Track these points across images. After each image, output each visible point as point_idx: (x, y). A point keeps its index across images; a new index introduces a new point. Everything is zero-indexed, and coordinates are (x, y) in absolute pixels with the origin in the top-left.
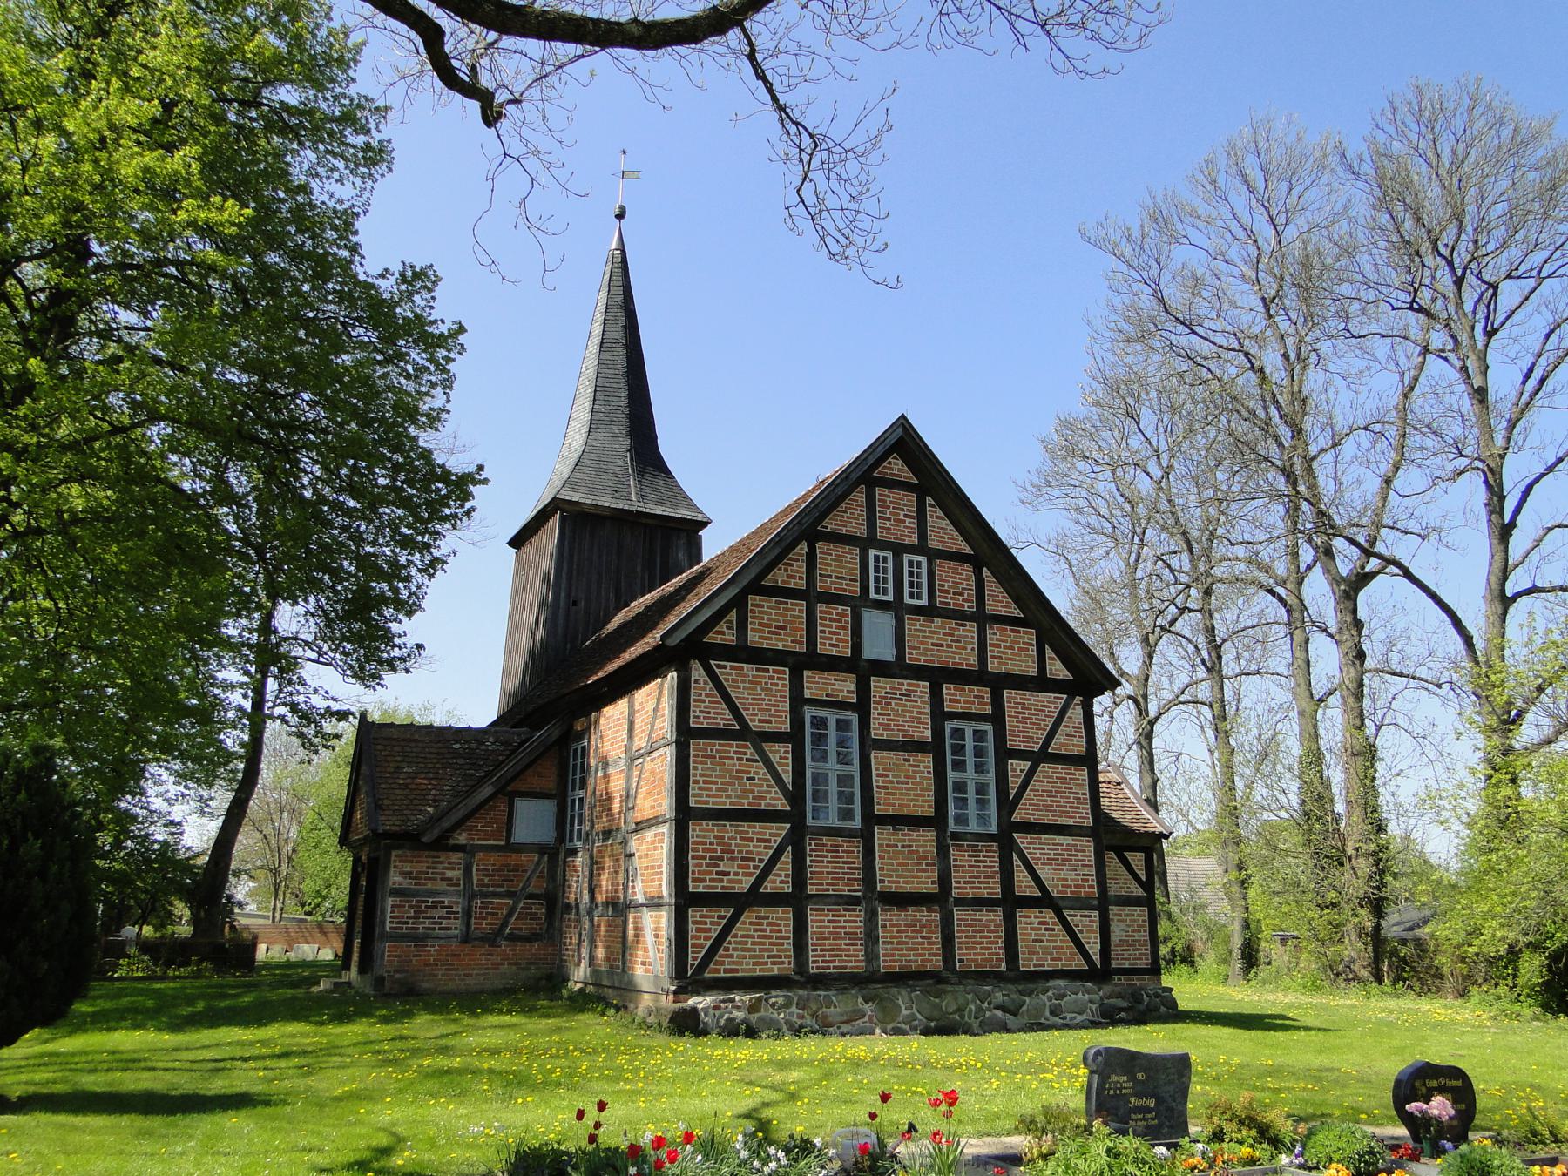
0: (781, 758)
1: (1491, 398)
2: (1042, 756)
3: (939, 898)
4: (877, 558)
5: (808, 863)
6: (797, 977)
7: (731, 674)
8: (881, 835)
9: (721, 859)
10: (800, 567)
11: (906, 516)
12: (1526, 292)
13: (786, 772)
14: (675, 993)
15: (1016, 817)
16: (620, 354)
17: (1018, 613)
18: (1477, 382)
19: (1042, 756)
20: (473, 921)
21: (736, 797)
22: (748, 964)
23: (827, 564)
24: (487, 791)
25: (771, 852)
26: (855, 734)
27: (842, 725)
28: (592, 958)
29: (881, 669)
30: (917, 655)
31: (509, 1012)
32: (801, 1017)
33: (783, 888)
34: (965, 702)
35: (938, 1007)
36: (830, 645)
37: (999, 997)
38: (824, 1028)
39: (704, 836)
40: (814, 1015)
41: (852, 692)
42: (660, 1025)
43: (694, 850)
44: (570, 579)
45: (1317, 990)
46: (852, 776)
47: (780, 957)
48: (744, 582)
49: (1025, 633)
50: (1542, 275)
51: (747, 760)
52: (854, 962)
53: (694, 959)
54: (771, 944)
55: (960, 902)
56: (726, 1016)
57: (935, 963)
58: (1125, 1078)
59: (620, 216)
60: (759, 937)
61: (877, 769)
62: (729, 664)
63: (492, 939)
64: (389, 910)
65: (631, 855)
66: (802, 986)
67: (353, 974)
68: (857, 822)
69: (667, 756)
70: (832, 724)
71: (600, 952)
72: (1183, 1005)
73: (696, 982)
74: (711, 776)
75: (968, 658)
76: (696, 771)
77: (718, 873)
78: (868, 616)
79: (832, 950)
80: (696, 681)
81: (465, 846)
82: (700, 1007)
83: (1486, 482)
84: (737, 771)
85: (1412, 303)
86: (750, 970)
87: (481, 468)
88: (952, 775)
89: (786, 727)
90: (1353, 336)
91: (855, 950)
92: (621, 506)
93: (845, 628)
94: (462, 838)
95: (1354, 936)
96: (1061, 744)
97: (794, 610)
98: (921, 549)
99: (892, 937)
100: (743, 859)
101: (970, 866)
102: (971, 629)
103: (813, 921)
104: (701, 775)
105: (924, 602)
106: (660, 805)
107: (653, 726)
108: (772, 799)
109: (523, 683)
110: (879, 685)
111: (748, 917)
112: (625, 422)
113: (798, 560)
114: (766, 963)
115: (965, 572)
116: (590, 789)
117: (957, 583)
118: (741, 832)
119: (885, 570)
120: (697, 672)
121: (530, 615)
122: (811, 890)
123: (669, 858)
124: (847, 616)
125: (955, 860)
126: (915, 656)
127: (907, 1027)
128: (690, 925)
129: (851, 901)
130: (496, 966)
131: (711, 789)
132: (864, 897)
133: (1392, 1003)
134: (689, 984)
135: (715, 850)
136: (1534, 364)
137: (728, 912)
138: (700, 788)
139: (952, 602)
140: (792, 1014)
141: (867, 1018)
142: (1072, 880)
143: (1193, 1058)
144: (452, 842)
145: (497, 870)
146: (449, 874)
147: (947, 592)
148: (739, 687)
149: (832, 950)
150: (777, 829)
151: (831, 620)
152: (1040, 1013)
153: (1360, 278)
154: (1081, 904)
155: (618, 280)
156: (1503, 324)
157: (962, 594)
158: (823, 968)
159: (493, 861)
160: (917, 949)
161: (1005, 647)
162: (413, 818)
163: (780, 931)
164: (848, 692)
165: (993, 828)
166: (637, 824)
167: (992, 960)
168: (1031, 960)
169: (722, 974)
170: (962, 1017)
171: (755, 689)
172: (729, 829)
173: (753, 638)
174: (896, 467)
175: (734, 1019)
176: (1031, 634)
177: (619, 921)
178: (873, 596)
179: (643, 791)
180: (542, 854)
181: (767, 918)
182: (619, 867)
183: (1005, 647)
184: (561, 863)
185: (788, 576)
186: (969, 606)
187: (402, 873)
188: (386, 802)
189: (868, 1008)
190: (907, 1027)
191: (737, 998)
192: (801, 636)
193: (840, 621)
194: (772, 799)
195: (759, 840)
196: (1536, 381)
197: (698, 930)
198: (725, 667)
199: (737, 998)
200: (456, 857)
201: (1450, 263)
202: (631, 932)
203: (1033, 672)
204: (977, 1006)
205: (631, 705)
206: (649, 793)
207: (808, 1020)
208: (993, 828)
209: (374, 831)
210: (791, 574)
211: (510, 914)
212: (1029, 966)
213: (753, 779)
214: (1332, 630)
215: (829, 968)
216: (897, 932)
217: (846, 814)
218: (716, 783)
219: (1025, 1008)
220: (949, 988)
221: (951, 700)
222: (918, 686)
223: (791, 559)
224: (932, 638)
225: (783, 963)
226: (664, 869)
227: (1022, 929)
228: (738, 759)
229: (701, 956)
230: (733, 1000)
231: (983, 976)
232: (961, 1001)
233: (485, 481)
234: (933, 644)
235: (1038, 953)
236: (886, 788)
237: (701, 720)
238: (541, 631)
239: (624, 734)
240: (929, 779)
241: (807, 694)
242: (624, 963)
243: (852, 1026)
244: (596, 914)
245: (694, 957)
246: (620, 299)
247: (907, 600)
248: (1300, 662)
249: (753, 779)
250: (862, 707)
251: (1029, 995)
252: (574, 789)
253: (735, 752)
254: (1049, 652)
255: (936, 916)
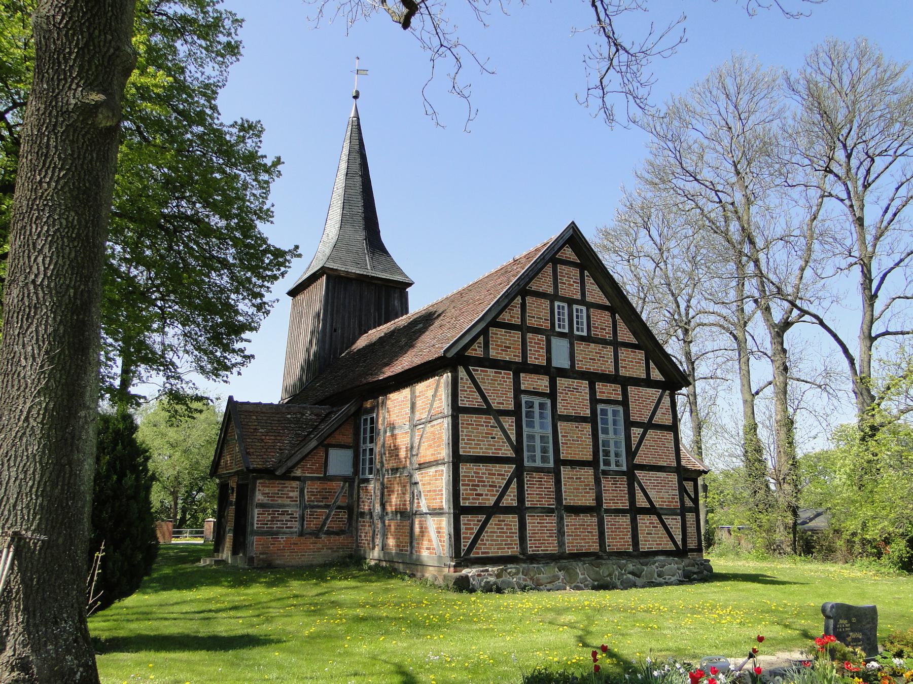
0: (509, 425)
1: (865, 224)
2: (649, 426)
3: (596, 509)
4: (559, 306)
5: (526, 488)
6: (521, 556)
7: (481, 375)
8: (565, 471)
9: (478, 486)
10: (517, 311)
11: (574, 282)
12: (887, 164)
13: (512, 434)
14: (455, 566)
15: (636, 461)
16: (358, 180)
17: (635, 341)
18: (858, 215)
19: (649, 426)
20: (305, 522)
21: (486, 449)
22: (494, 549)
23: (532, 310)
24: (314, 443)
25: (505, 482)
26: (548, 412)
27: (542, 406)
28: (384, 547)
29: (562, 373)
30: (582, 365)
31: (346, 579)
32: (525, 580)
33: (512, 503)
34: (608, 393)
35: (598, 573)
36: (535, 358)
37: (630, 567)
38: (537, 587)
39: (469, 472)
40: (532, 579)
41: (547, 387)
42: (447, 586)
43: (463, 481)
44: (332, 315)
45: (764, 559)
46: (548, 437)
47: (512, 544)
48: (489, 319)
49: (639, 353)
50: (897, 154)
51: (491, 426)
52: (552, 547)
53: (464, 546)
54: (507, 537)
55: (608, 511)
56: (485, 580)
57: (595, 547)
58: (846, 621)
59: (356, 97)
60: (500, 532)
61: (561, 433)
62: (479, 369)
63: (316, 534)
64: (256, 516)
65: (416, 483)
66: (524, 561)
67: (226, 554)
68: (551, 464)
69: (446, 423)
70: (536, 406)
71: (391, 542)
72: (716, 570)
73: (466, 559)
74: (471, 436)
75: (608, 367)
76: (463, 433)
77: (477, 495)
78: (555, 341)
79: (540, 540)
80: (462, 379)
81: (300, 477)
82: (470, 575)
83: (862, 271)
84: (486, 433)
85: (826, 167)
86: (495, 552)
87: (297, 247)
88: (601, 437)
89: (511, 407)
90: (789, 186)
91: (552, 540)
92: (362, 273)
93: (542, 348)
94: (298, 473)
95: (782, 529)
96: (659, 419)
97: (515, 337)
98: (582, 302)
99: (572, 532)
100: (490, 486)
101: (613, 490)
102: (610, 349)
103: (529, 523)
104: (466, 436)
105: (585, 334)
106: (439, 453)
107: (432, 405)
108: (505, 450)
109: (301, 379)
110: (562, 383)
111: (493, 521)
112: (362, 222)
113: (516, 307)
114: (504, 548)
115: (607, 315)
116: (380, 443)
117: (602, 322)
118: (490, 470)
119: (563, 314)
120: (462, 373)
121: (305, 337)
122: (528, 504)
123: (447, 485)
124: (543, 341)
125: (604, 487)
126: (581, 366)
127: (582, 585)
128: (462, 526)
129: (550, 511)
130: (319, 550)
131: (471, 444)
132: (556, 508)
133: (808, 566)
134: (463, 561)
135: (474, 481)
136: (889, 205)
137: (483, 517)
138: (465, 443)
139: (600, 334)
140: (520, 579)
141: (560, 581)
142: (667, 498)
143: (878, 607)
144: (293, 475)
145: (319, 492)
146: (291, 494)
147: (597, 328)
148: (485, 383)
149: (540, 540)
150: (509, 467)
151: (535, 343)
152: (652, 574)
153: (799, 152)
154: (672, 512)
155: (356, 136)
156: (873, 181)
157: (605, 329)
158: (535, 551)
159: (317, 486)
160: (585, 539)
161: (628, 361)
162: (269, 460)
163: (511, 529)
164: (545, 386)
165: (624, 468)
166: (419, 464)
167: (625, 545)
168: (646, 545)
169: (480, 555)
170: (611, 579)
171: (494, 384)
172: (482, 468)
173: (493, 353)
174: (568, 253)
175: (489, 582)
176: (642, 353)
177: (408, 523)
178: (557, 329)
179: (424, 445)
180: (345, 482)
181: (504, 521)
182: (406, 490)
183: (628, 361)
184: (356, 487)
185: (511, 316)
186: (609, 337)
187: (263, 494)
188: (252, 450)
189: (561, 574)
190: (582, 585)
191: (490, 569)
192: (519, 353)
193: (540, 344)
194: (505, 450)
195: (499, 475)
196: (891, 215)
197: (466, 529)
198: (477, 370)
199: (490, 569)
200: (295, 484)
201: (845, 146)
202: (417, 529)
203: (644, 376)
204: (619, 573)
205: (413, 393)
206: (430, 446)
207: (529, 582)
208: (624, 468)
209: (247, 468)
210: (512, 316)
211: (327, 519)
212: (644, 548)
213: (495, 438)
214: (769, 353)
215: (538, 551)
216: (575, 529)
217: (544, 459)
218: (474, 440)
219: (644, 573)
220: (604, 562)
221: (600, 392)
222: (582, 383)
223: (512, 306)
224: (589, 355)
225: (514, 548)
226: (444, 492)
227: (641, 527)
228: (486, 426)
229: (468, 544)
230: (487, 571)
231: (620, 554)
232: (611, 569)
233: (300, 256)
234: (590, 359)
235: (649, 541)
236: (567, 444)
237: (465, 402)
238: (314, 348)
239: (408, 411)
240: (589, 438)
241: (523, 388)
242: (412, 547)
243: (553, 586)
244: (387, 518)
245: (465, 545)
246: (357, 147)
247: (576, 332)
248: (745, 372)
249: (495, 438)
250: (552, 395)
251: (646, 565)
252: (365, 442)
253: (484, 422)
254: (652, 364)
255: (595, 519)
